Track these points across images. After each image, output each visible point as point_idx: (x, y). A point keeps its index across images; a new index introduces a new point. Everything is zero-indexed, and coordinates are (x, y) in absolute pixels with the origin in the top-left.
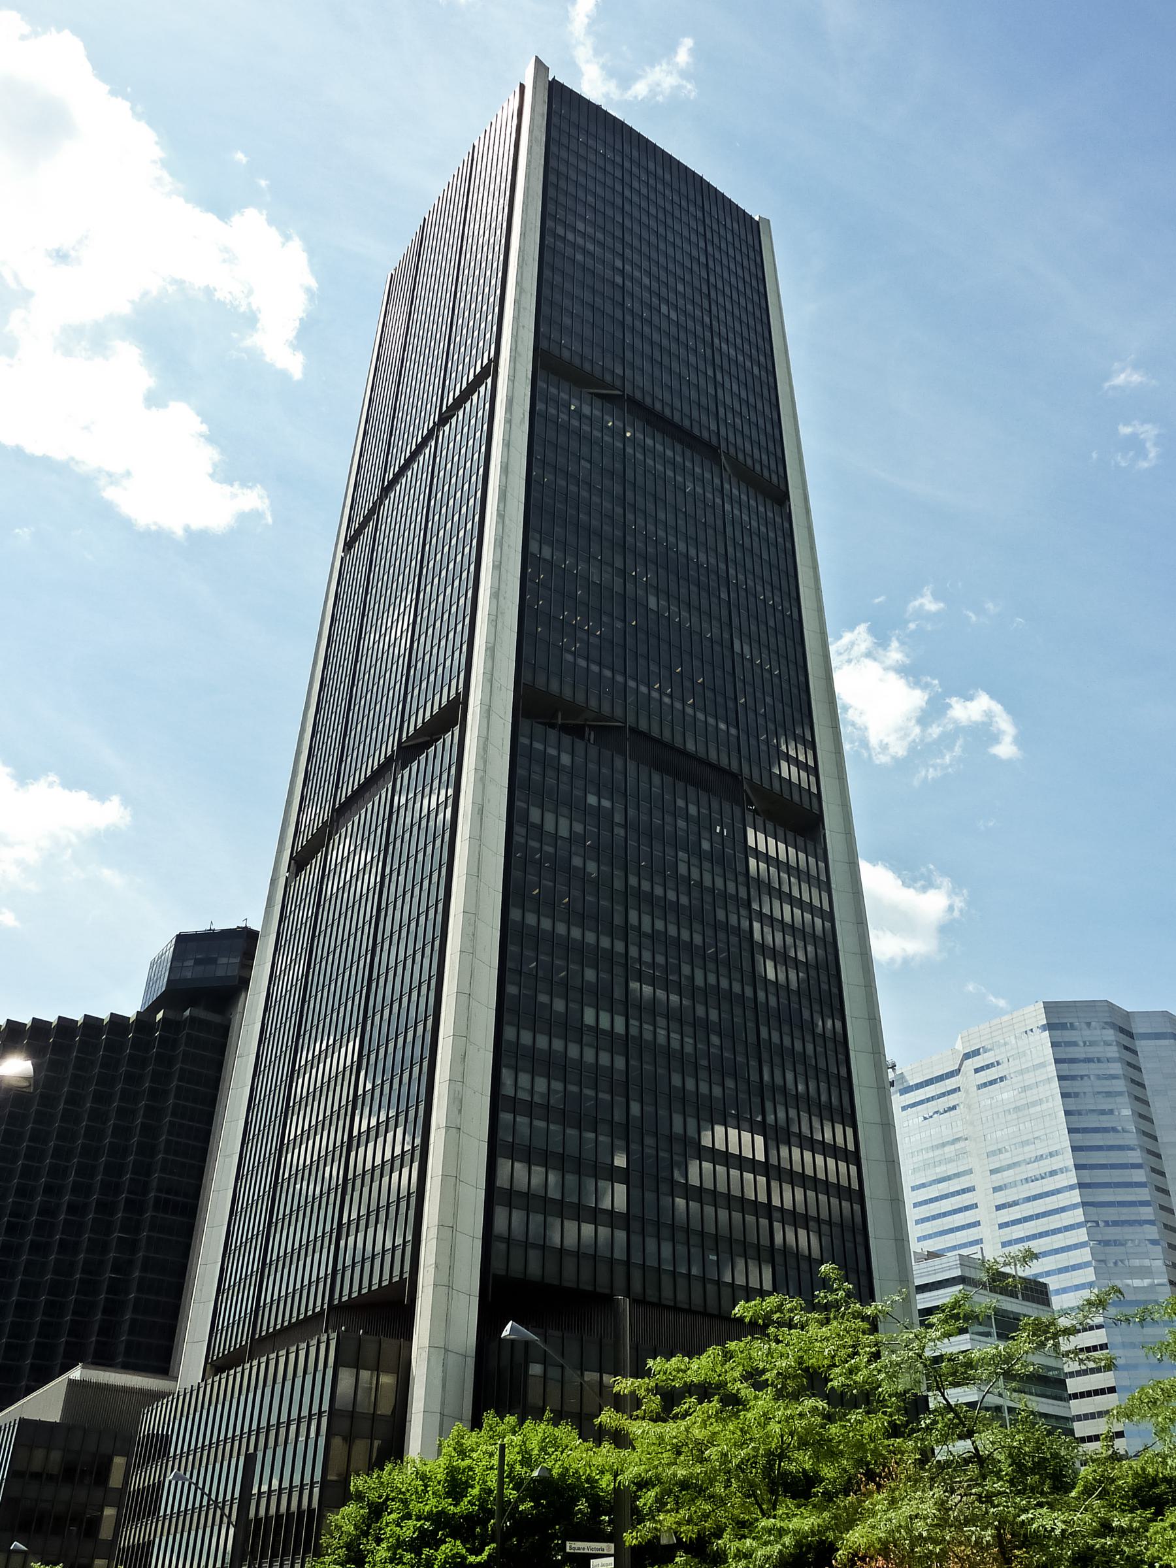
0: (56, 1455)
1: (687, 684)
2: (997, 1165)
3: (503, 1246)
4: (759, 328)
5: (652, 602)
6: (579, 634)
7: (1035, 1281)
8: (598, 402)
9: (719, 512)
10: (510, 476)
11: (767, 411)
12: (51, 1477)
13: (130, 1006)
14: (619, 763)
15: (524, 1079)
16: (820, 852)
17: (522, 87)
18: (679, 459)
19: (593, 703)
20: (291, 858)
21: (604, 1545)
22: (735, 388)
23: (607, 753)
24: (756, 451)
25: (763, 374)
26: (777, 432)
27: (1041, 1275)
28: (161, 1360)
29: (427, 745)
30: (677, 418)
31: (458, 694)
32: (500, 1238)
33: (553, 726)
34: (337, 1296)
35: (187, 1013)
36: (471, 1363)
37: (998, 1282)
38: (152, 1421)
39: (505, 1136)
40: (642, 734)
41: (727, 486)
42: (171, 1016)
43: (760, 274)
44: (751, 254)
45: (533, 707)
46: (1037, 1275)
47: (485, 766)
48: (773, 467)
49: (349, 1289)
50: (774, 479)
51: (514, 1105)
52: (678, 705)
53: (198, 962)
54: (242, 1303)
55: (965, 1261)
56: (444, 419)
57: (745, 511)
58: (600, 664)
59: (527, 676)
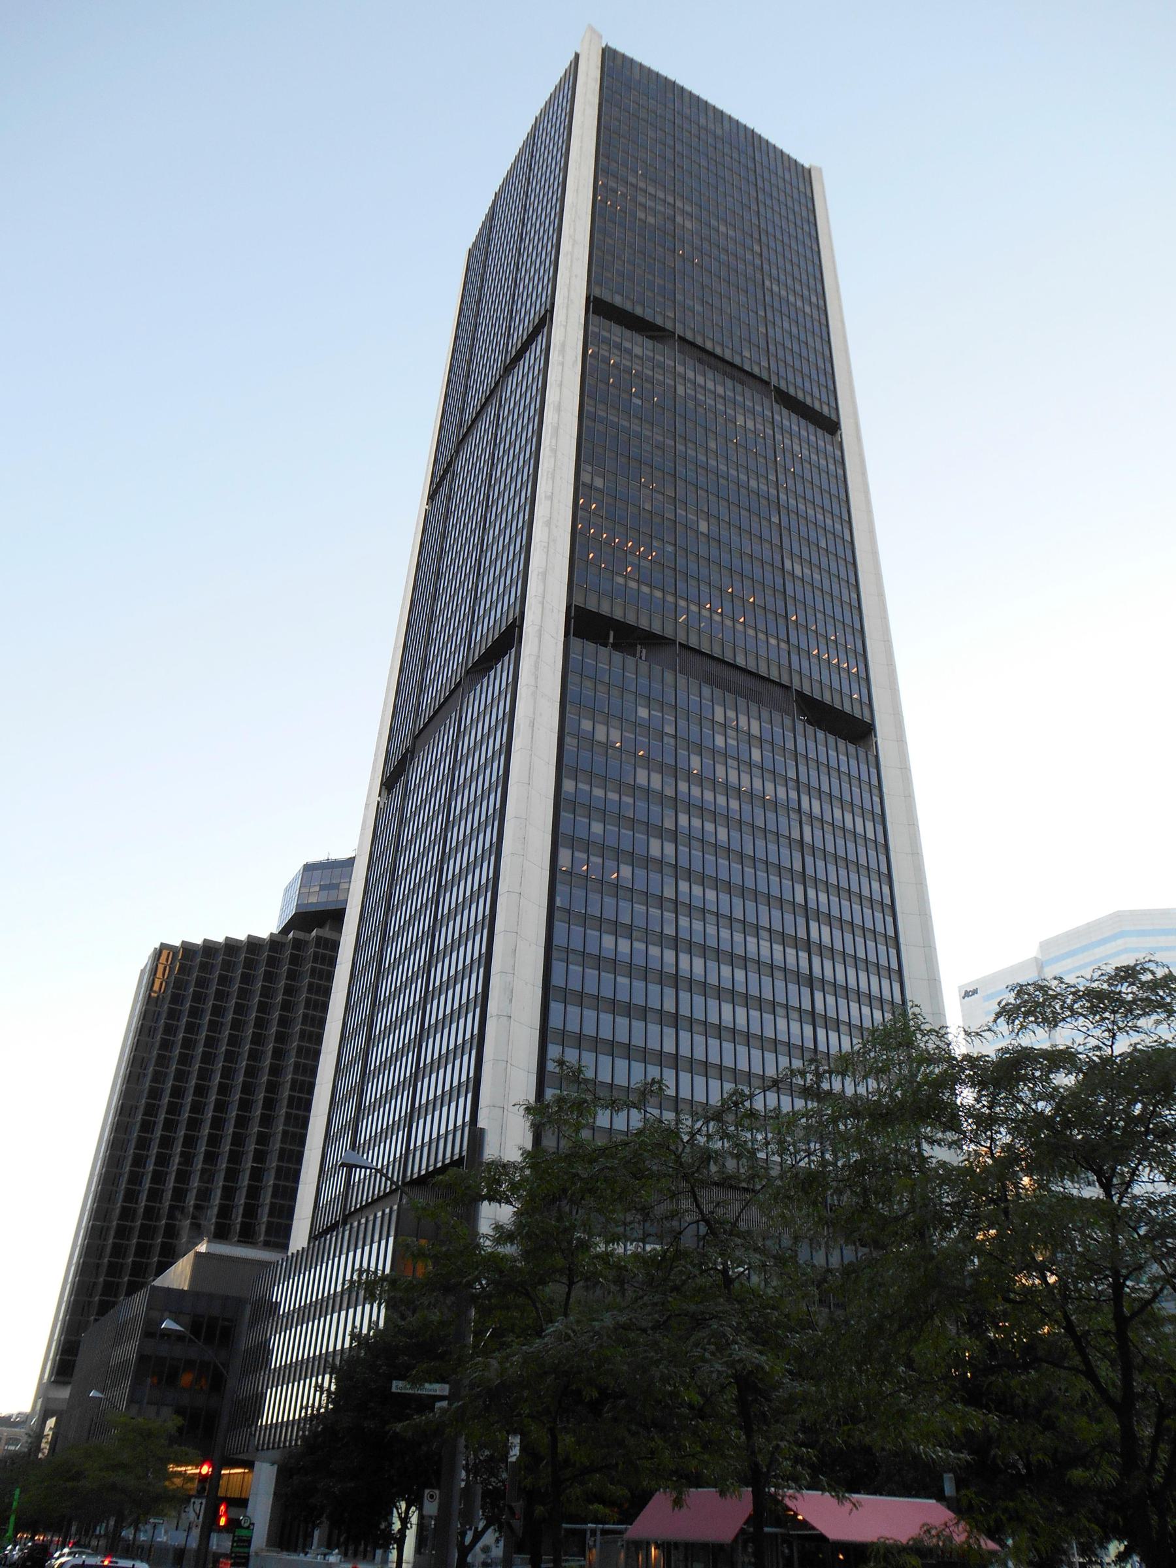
1: (738, 602)
4: (810, 269)
5: (703, 527)
6: (630, 558)
9: (769, 442)
11: (819, 347)
14: (669, 677)
16: (871, 759)
18: (730, 394)
21: (437, 1386)
22: (786, 325)
23: (657, 669)
24: (807, 385)
25: (815, 312)
26: (828, 365)
28: (280, 1234)
31: (515, 619)
34: (409, 1174)
35: (314, 933)
41: (777, 417)
43: (811, 219)
45: (583, 624)
47: (536, 682)
48: (824, 398)
49: (419, 1166)
51: (566, 995)
52: (728, 623)
53: (322, 888)
54: (336, 1185)
57: (796, 441)
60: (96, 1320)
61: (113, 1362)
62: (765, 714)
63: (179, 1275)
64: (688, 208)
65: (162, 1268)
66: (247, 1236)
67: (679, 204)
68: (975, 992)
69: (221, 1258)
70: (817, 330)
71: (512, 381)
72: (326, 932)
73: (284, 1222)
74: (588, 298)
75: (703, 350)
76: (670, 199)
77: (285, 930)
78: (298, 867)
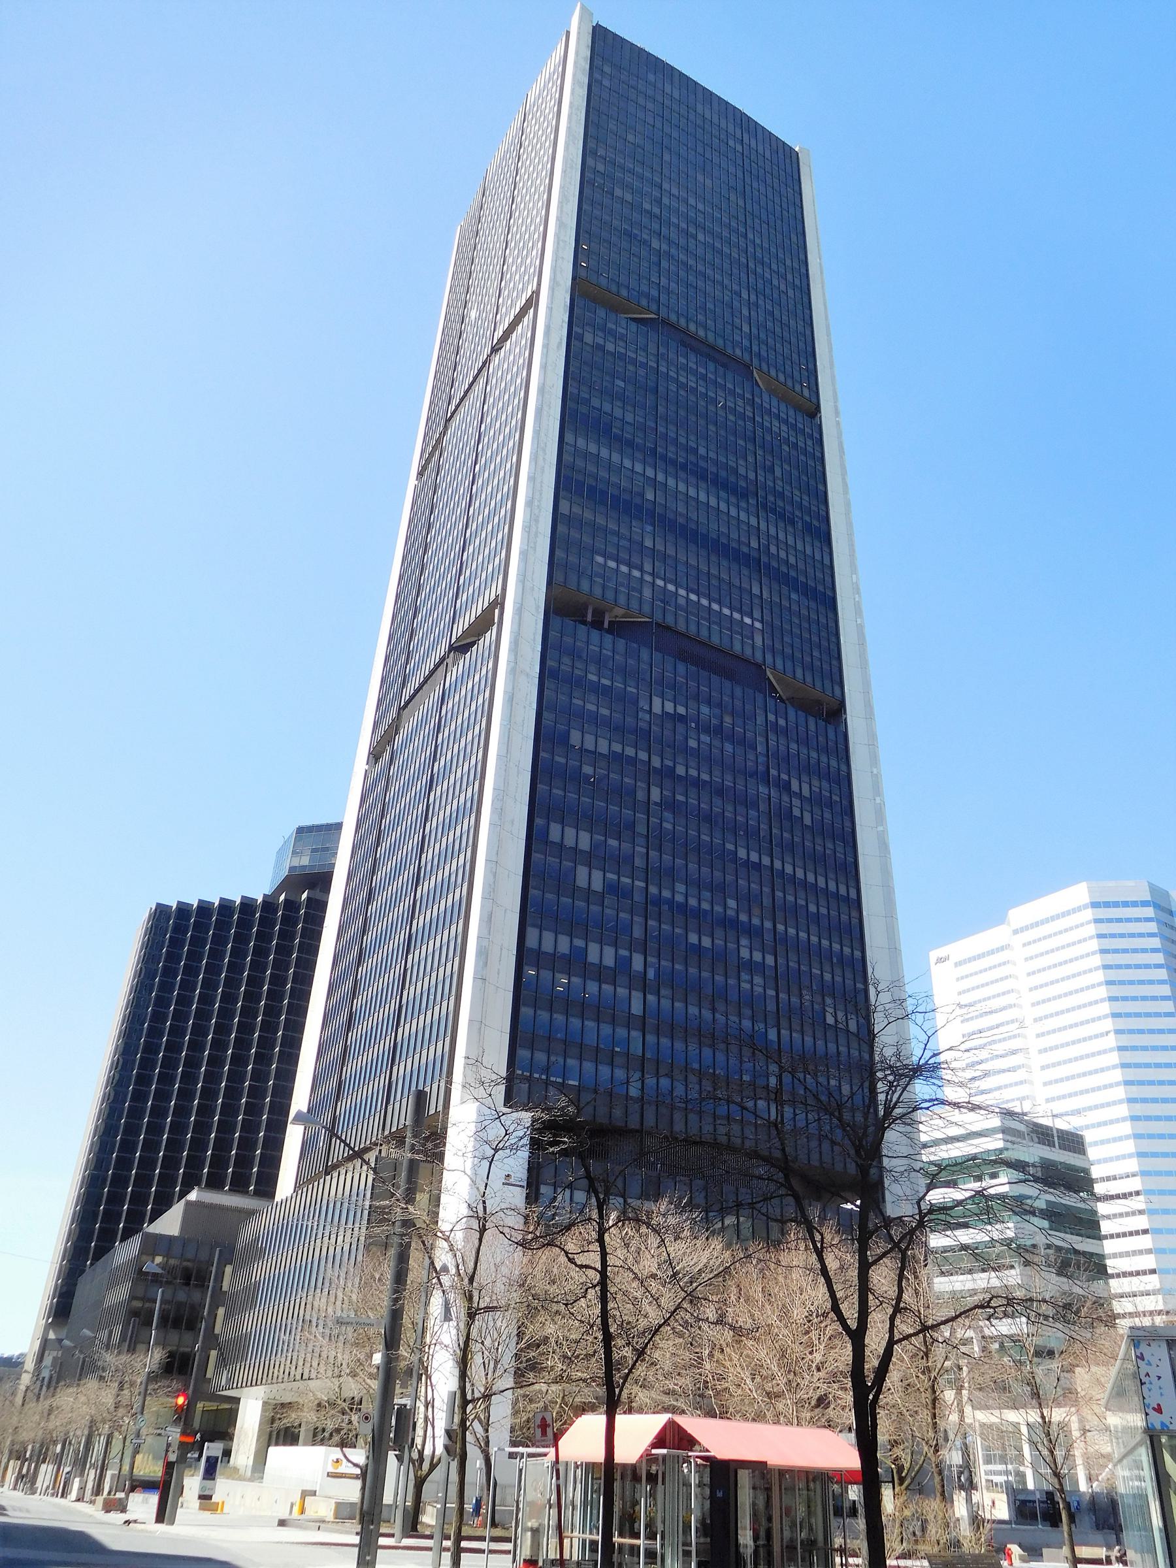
8: (633, 326)
15: (548, 937)
27: (1082, 1128)
28: (267, 1187)
29: (472, 644)
30: (711, 337)
31: (497, 596)
33: (584, 623)
37: (1043, 1135)
40: (668, 628)
44: (790, 182)
50: (806, 393)
56: (495, 350)
58: (730, 608)
59: (559, 577)
60: (92, 1264)
61: (106, 1305)
63: (170, 1223)
64: (675, 191)
65: (156, 1215)
66: (239, 1186)
67: (666, 186)
69: (212, 1207)
70: (799, 312)
71: (496, 360)
73: (171, 1172)
75: (685, 332)
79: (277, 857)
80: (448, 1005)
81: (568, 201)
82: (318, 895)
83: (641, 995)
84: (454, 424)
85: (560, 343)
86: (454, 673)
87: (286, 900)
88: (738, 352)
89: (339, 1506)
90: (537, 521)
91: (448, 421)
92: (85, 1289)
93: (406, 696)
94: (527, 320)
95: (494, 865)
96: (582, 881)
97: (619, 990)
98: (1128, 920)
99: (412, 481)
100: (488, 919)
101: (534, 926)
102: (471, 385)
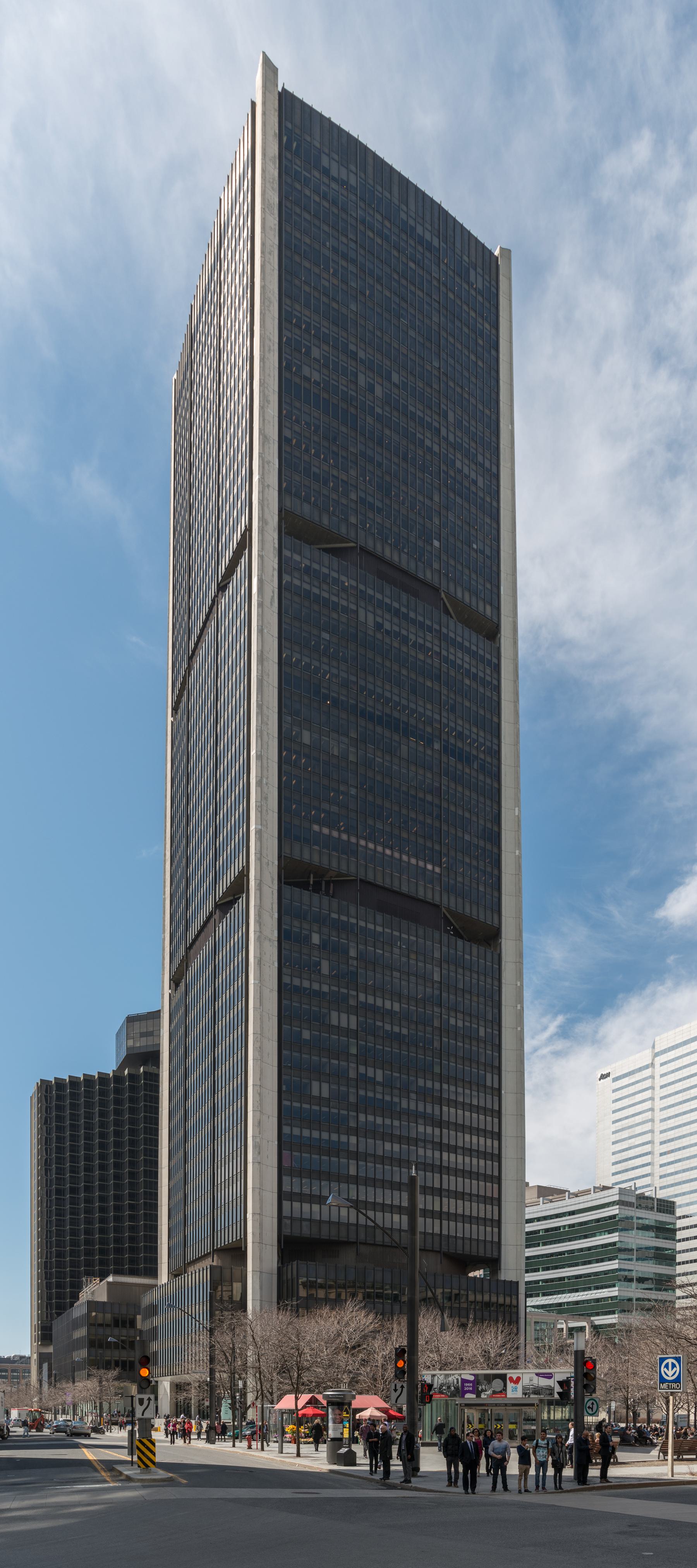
0: (108, 1316)
2: (665, 1127)
3: (288, 1222)
7: (667, 1201)
10: (265, 663)
12: (108, 1325)
13: (109, 1066)
16: (496, 957)
17: (253, 104)
19: (334, 864)
20: (170, 980)
32: (286, 1217)
36: (275, 1278)
37: (644, 1202)
38: (148, 1299)
39: (286, 1164)
40: (369, 883)
42: (133, 1072)
45: (293, 876)
46: (669, 1197)
55: (622, 1191)
56: (222, 588)
59: (287, 850)
62: (421, 932)
68: (608, 1075)
71: (223, 602)
72: (151, 1069)
74: (280, 511)
76: (421, 818)
77: (121, 1067)
78: (123, 1019)
79: (117, 1039)
80: (237, 1188)
81: (268, 402)
82: (151, 1069)
83: (355, 1162)
84: (198, 660)
85: (273, 597)
86: (221, 928)
87: (129, 1074)
88: (429, 575)
89: (583, 1352)
90: (266, 798)
91: (191, 658)
92: (59, 1326)
93: (191, 935)
94: (243, 561)
95: (258, 1088)
96: (315, 1092)
97: (341, 1160)
98: (627, 1118)
99: (170, 719)
100: (258, 1124)
101: (286, 1125)
102: (205, 623)
